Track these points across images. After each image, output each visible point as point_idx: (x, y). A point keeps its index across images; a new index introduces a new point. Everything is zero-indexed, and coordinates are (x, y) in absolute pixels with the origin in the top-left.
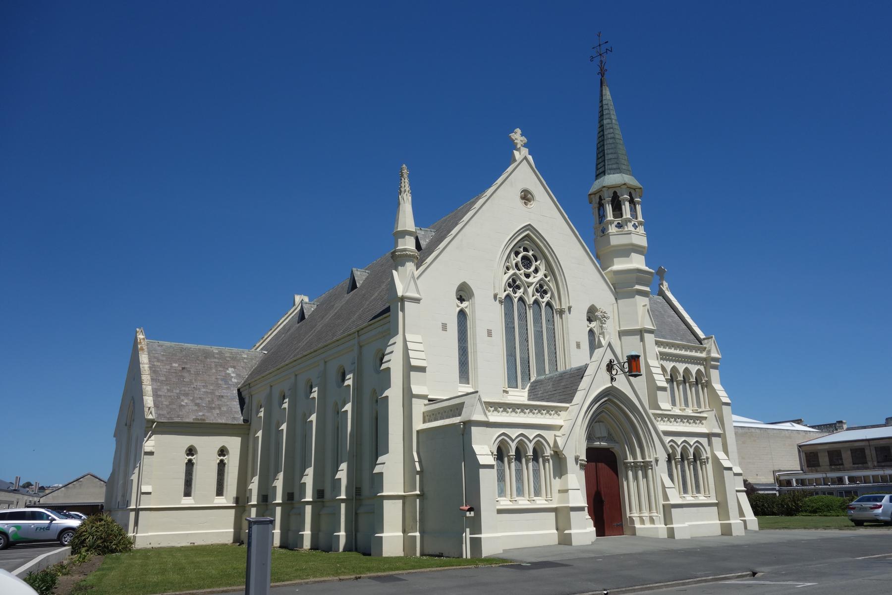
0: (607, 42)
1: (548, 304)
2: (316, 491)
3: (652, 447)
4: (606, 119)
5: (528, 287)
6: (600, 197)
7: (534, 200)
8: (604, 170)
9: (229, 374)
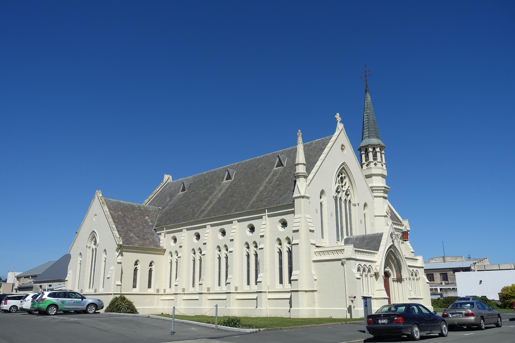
5: (343, 192)
8: (368, 135)
9: (147, 220)
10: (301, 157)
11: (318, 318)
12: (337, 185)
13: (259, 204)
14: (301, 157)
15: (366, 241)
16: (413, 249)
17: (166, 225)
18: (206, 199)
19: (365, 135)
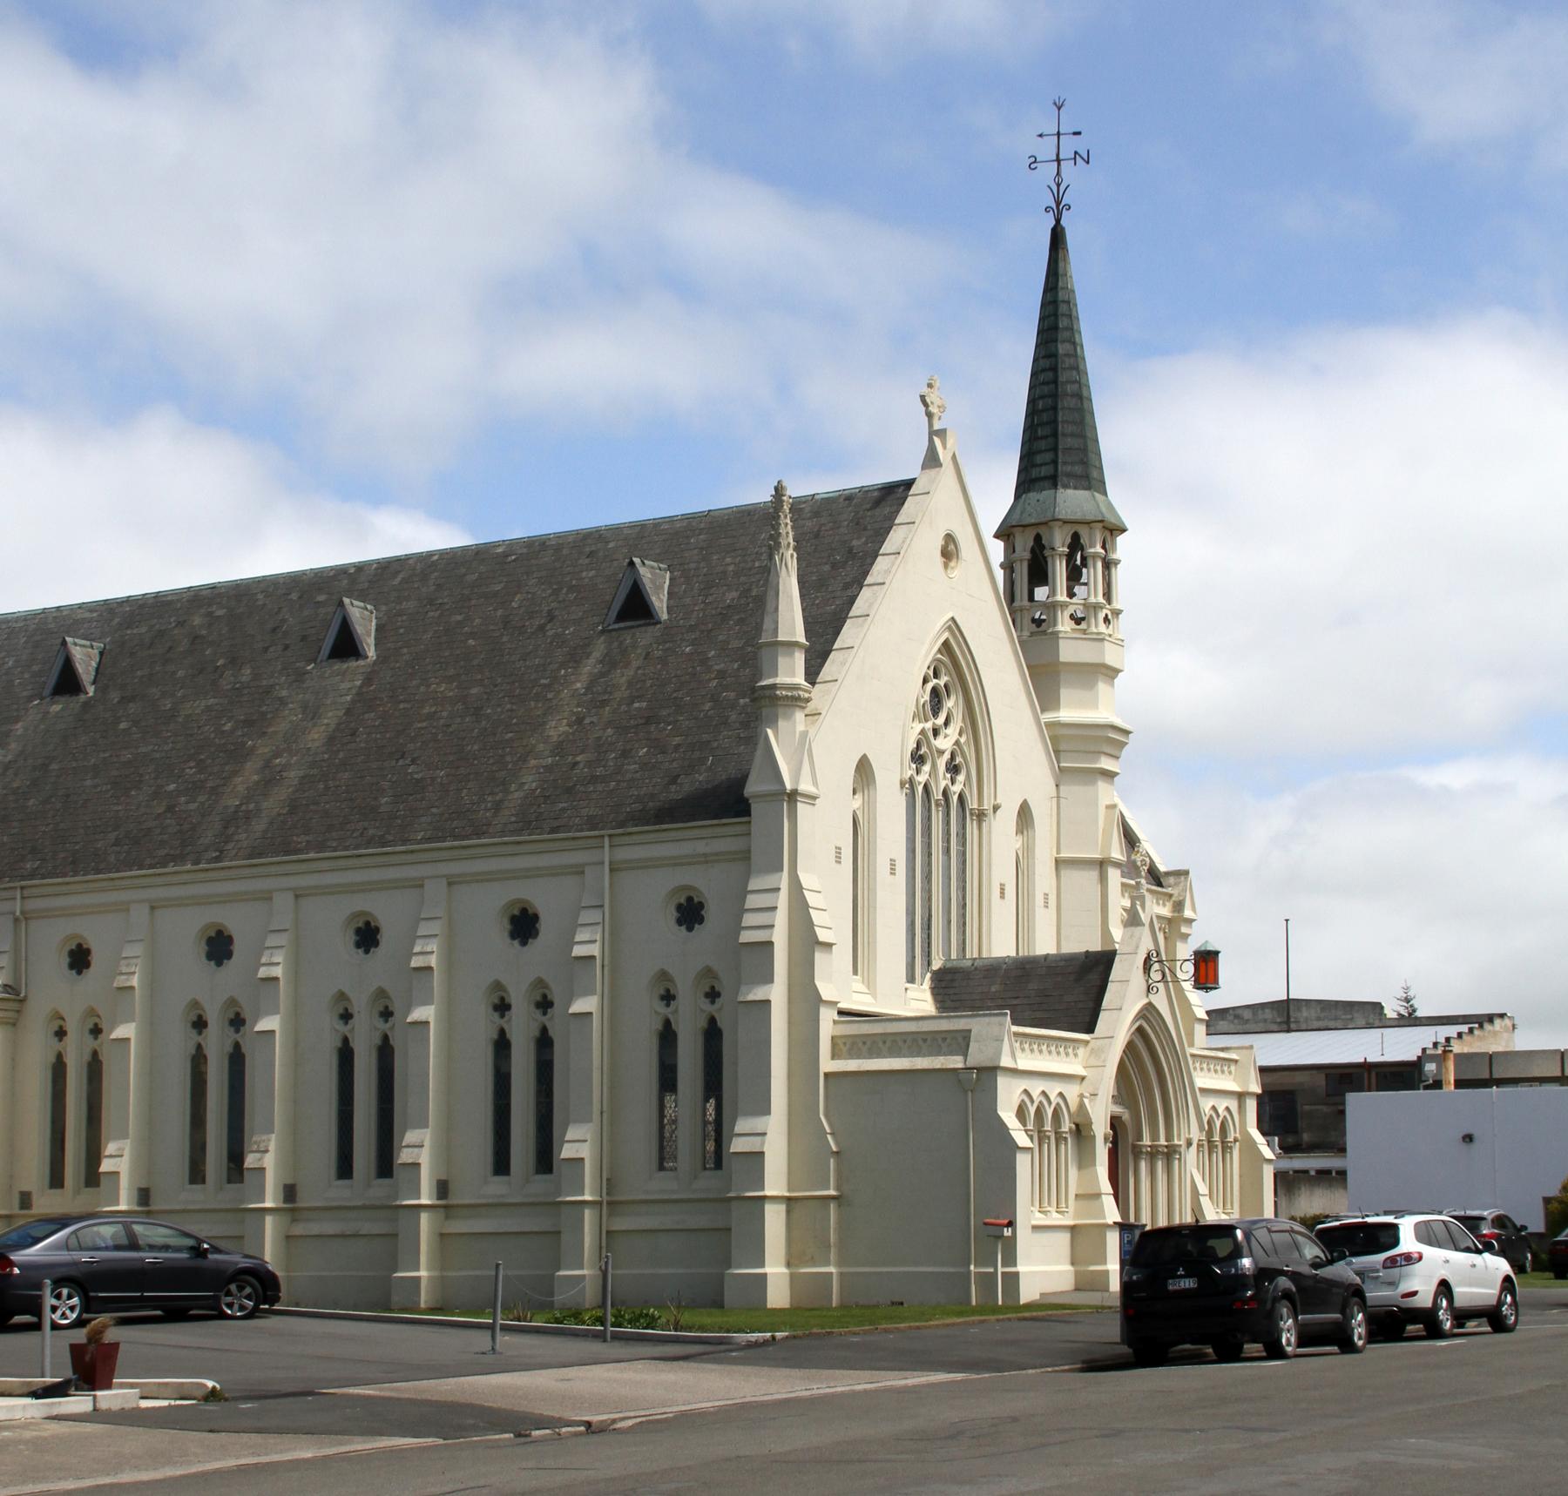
0: (1079, 133)
1: (961, 798)
2: (435, 1182)
3: (1183, 1112)
4: (1064, 341)
6: (1038, 538)
7: (958, 558)
10: (791, 619)
11: (778, 1307)
12: (918, 727)
13: (563, 810)
14: (791, 619)
15: (1033, 986)
16: (1183, 989)
17: (23, 878)
18: (238, 755)
19: (1038, 469)
